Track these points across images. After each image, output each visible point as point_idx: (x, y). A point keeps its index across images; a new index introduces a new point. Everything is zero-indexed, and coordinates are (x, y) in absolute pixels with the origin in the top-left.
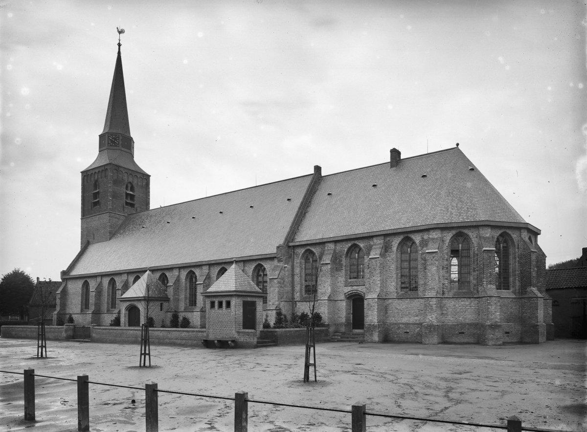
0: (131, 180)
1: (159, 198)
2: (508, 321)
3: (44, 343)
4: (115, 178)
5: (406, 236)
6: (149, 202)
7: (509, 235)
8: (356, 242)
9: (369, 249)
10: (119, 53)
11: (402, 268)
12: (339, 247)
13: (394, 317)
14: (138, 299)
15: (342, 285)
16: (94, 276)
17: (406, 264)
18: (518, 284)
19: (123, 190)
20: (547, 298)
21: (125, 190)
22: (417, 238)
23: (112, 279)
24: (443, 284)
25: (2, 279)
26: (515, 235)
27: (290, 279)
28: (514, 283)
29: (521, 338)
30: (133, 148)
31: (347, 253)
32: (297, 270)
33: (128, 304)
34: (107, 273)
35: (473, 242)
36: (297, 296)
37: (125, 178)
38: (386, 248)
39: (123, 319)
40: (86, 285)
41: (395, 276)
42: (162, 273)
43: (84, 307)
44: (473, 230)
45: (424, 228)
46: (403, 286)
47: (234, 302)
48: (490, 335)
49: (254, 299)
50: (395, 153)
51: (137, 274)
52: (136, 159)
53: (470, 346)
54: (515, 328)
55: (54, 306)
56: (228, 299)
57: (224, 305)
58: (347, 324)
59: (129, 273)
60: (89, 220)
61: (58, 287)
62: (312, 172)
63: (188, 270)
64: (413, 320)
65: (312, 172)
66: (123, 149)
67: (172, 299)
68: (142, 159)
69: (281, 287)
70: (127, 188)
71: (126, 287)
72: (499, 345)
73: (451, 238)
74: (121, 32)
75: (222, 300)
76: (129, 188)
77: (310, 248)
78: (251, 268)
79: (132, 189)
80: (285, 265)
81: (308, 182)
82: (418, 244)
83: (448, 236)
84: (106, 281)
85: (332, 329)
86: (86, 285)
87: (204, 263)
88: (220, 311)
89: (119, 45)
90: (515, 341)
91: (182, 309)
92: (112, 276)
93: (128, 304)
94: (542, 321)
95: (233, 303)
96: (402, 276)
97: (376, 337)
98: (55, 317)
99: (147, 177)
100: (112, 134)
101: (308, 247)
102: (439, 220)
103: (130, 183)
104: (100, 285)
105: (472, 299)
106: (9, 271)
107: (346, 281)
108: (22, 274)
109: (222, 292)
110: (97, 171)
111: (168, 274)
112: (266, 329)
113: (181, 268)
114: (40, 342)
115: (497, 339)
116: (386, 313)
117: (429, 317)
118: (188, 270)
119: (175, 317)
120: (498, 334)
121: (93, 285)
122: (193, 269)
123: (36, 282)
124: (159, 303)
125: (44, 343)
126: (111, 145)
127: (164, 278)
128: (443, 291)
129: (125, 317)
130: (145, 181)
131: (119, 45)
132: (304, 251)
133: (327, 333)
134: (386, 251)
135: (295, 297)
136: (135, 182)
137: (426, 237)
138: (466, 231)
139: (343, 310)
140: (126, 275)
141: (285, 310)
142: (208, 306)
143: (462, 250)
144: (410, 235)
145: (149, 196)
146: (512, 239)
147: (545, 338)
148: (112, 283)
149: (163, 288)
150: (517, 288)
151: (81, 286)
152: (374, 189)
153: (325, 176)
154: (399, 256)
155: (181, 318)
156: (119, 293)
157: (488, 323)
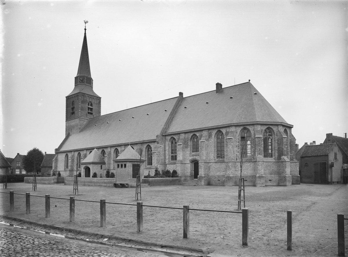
0: (91, 100)
1: (105, 110)
2: (271, 174)
3: (35, 184)
4: (82, 100)
5: (219, 129)
6: (100, 112)
7: (272, 129)
8: (195, 133)
9: (201, 136)
10: (85, 34)
11: (217, 147)
12: (187, 135)
13: (213, 172)
14: (90, 163)
15: (189, 156)
16: (70, 151)
17: (219, 145)
18: (277, 154)
19: (87, 106)
20: (296, 162)
21: (87, 106)
22: (224, 131)
23: (103, 150)
24: (237, 155)
25: (28, 153)
26: (275, 129)
27: (164, 152)
28: (275, 154)
29: (279, 183)
30: (92, 83)
31: (191, 139)
32: (167, 148)
33: (84, 166)
34: (76, 150)
35: (252, 132)
36: (167, 161)
37: (88, 99)
38: (210, 136)
39: (83, 174)
40: (67, 156)
41: (213, 151)
42: (103, 149)
43: (66, 167)
44: (251, 126)
45: (222, 126)
46: (218, 156)
47: (128, 164)
48: (258, 181)
49: (139, 163)
50: (219, 85)
51: (90, 150)
52: (94, 89)
53: (250, 187)
54: (275, 177)
55: (51, 167)
56: (125, 163)
57: (123, 166)
58: (191, 176)
59: (87, 149)
60: (69, 122)
61: (54, 157)
62: (178, 95)
63: (115, 148)
64: (222, 174)
65: (178, 95)
66: (87, 84)
67: (106, 163)
68: (97, 89)
69: (158, 157)
70: (88, 105)
71: (85, 156)
72: (263, 187)
73: (240, 131)
74: (86, 22)
75: (122, 164)
76: (90, 105)
77: (195, 133)
78: (101, 150)
79: (91, 105)
80: (161, 145)
81: (175, 101)
82: (224, 134)
83: (239, 129)
84: (76, 154)
85: (183, 179)
86: (67, 156)
87: (122, 144)
88: (122, 169)
89: (85, 29)
90: (275, 184)
91: (112, 168)
92: (79, 151)
93: (84, 166)
94: (289, 174)
95: (127, 165)
96: (217, 151)
97: (203, 183)
98: (52, 173)
99: (99, 99)
100: (81, 77)
101: (172, 136)
102: (235, 121)
103: (90, 102)
104: (73, 156)
105: (251, 163)
106: (31, 149)
107: (190, 154)
108: (38, 150)
109: (122, 160)
110: (73, 96)
111: (105, 150)
112: (145, 179)
113: (111, 147)
114: (34, 184)
115: (262, 183)
116: (209, 170)
117: (228, 172)
118: (115, 148)
119: (108, 172)
120: (263, 181)
121: (70, 155)
122: (117, 148)
123: (44, 154)
124: (100, 165)
125: (35, 184)
126: (80, 83)
127: (117, 151)
128: (236, 158)
129: (83, 172)
130: (98, 101)
131: (85, 29)
132: (170, 138)
133: (180, 181)
134: (209, 138)
135: (166, 162)
136: (93, 102)
137: (228, 130)
138: (248, 127)
139: (189, 169)
140: (85, 151)
141: (160, 169)
142: (116, 166)
143: (246, 137)
144: (220, 129)
145: (101, 109)
146: (273, 131)
147: (291, 183)
148: (79, 154)
149: (103, 157)
150: (276, 156)
151: (64, 156)
152: (207, 105)
153: (185, 98)
154: (216, 140)
155: (110, 173)
156: (81, 160)
157: (258, 175)
